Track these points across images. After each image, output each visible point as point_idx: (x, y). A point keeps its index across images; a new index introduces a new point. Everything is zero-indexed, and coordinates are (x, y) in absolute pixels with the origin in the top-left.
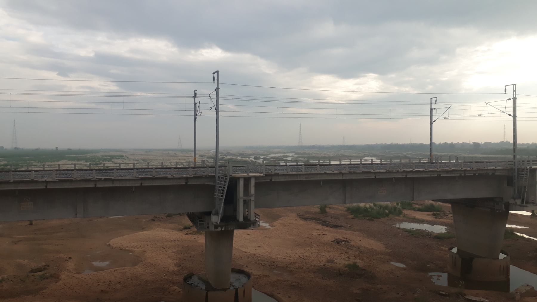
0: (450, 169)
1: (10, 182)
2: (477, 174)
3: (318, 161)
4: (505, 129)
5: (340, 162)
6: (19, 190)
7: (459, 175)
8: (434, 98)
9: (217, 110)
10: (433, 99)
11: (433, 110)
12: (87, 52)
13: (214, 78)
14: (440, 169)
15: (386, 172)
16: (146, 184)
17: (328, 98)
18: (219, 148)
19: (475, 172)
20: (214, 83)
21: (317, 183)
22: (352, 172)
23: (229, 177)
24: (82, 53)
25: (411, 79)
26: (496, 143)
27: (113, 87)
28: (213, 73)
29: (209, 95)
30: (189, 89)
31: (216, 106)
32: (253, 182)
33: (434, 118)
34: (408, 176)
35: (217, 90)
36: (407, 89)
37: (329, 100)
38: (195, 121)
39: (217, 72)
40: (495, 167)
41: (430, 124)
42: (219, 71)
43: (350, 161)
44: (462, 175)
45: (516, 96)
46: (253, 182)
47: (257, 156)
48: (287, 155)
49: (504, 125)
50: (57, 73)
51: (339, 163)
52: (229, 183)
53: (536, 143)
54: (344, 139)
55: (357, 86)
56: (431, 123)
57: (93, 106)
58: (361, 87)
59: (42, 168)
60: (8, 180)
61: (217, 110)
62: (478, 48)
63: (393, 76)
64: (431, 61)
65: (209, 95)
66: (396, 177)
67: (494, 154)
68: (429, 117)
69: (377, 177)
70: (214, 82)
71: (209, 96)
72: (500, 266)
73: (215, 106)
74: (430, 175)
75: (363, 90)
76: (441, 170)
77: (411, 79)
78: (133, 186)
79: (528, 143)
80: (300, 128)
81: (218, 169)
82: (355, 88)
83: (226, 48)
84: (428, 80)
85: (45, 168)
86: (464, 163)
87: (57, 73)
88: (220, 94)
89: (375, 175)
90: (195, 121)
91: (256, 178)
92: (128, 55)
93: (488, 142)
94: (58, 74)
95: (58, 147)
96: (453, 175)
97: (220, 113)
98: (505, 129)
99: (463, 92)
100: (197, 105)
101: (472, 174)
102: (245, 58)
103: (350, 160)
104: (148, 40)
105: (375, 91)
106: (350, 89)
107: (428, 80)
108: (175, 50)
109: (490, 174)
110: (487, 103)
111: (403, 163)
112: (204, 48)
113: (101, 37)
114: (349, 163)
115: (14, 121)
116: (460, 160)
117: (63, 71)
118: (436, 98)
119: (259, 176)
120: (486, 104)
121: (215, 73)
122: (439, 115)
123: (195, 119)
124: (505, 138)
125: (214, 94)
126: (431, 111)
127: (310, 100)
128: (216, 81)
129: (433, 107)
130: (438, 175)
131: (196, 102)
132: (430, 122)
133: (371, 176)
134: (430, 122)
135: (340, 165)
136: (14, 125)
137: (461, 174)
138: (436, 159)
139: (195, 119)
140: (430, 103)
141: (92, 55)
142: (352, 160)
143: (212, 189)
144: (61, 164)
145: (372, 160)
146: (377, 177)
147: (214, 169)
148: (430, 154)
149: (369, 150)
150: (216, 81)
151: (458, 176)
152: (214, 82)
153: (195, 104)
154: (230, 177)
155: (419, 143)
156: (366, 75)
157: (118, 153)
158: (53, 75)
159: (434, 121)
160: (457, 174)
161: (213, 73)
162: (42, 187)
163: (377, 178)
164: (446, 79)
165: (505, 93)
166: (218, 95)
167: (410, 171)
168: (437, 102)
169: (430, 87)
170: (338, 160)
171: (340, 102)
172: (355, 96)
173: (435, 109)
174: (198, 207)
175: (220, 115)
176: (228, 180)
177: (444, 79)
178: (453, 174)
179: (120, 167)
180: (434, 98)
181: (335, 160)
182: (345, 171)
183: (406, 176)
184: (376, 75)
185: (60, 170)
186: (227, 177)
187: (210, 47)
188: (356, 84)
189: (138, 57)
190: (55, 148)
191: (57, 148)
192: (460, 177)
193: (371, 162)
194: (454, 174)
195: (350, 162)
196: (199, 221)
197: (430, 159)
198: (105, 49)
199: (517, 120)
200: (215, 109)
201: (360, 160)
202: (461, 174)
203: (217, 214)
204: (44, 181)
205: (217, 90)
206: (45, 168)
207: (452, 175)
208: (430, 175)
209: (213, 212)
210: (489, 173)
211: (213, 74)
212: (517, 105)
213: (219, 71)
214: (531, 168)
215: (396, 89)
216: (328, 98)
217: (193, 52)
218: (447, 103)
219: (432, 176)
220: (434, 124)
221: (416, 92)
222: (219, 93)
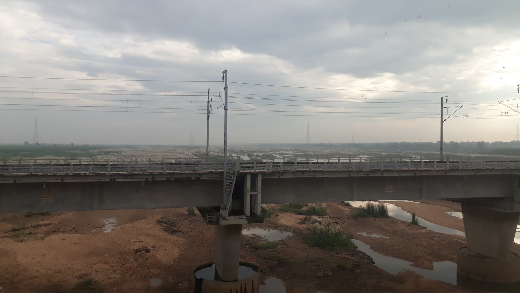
0: (128, 172)
1: (447, 170)
2: (172, 179)
3: (305, 159)
4: (517, 128)
5: (329, 160)
6: (467, 176)
7: (144, 180)
8: (445, 97)
9: (226, 109)
10: (443, 98)
11: (444, 109)
12: (114, 54)
13: (223, 77)
14: (111, 173)
15: (27, 176)
16: (418, 174)
17: (345, 97)
18: (228, 145)
19: (169, 177)
20: (223, 81)
21: (39, 185)
22: (373, 170)
23: (236, 173)
24: (110, 54)
25: (427, 78)
26: (507, 143)
27: (138, 87)
28: (223, 73)
29: (220, 94)
30: (204, 87)
31: (224, 105)
32: (260, 179)
33: (445, 117)
34: (65, 181)
35: (226, 88)
36: (424, 88)
37: (345, 99)
38: (208, 119)
39: (226, 71)
40: (199, 171)
41: (440, 123)
42: (227, 70)
43: (350, 160)
44: (149, 180)
45: (227, 85)
46: (260, 179)
47: (251, 153)
48: (283, 153)
49: (308, 122)
50: (87, 73)
51: (348, 161)
52: (236, 178)
53: (518, 143)
54: (353, 137)
55: (373, 85)
56: (442, 122)
57: (120, 104)
58: (377, 86)
59: (338, 160)
60: (309, 169)
61: (226, 109)
62: (496, 47)
63: (409, 75)
64: (448, 61)
65: (220, 94)
66: (47, 181)
67: (488, 154)
68: (440, 116)
69: (17, 182)
70: (223, 80)
71: (219, 95)
72: (231, 290)
73: (224, 104)
74: (100, 180)
75: (380, 89)
76: (112, 173)
77: (427, 78)
78: (325, 178)
79: (432, 141)
80: (308, 126)
81: (226, 166)
82: (371, 87)
83: (244, 49)
84: (445, 80)
85: (6, 163)
86: (327, 163)
87: (87, 73)
88: (228, 92)
89: (14, 180)
90: (208, 119)
91: (263, 174)
92: (153, 56)
93: (498, 142)
94: (87, 75)
95: (73, 142)
96: (136, 180)
97: (228, 112)
98: (517, 128)
99: (481, 91)
100: (210, 103)
101: (165, 179)
102: (263, 58)
103: (339, 158)
104: (171, 43)
105: (391, 90)
106: (367, 88)
107: (445, 80)
108: (196, 51)
109: (192, 179)
110: (500, 102)
111: (342, 163)
112: (224, 49)
113: (128, 39)
114: (327, 161)
115: (36, 118)
116: (432, 159)
117: (93, 71)
118: (446, 97)
119: (16, 175)
120: (499, 103)
121: (224, 73)
122: (450, 114)
123: (208, 116)
124: (518, 137)
125: (223, 94)
126: (441, 110)
127: (326, 99)
128: (225, 80)
129: (444, 107)
130: (111, 180)
131: (209, 101)
132: (441, 121)
133: (21, 180)
134: (440, 121)
135: (318, 163)
136: (36, 122)
137: (147, 179)
138: (447, 158)
139: (208, 116)
140: (441, 102)
141: (119, 56)
142: (340, 159)
143: (221, 183)
144: (362, 157)
145: (361, 158)
146: (17, 182)
147: (223, 165)
148: (441, 153)
149: (362, 148)
150: (225, 80)
151: (144, 181)
152: (223, 80)
153: (208, 102)
154: (237, 173)
155: (429, 142)
156: (383, 74)
157: (113, 150)
158: (83, 75)
159: (445, 120)
160: (142, 178)
161: (223, 73)
162: (12, 181)
163: (17, 183)
164: (463, 78)
165: (519, 93)
166: (226, 93)
167: (194, 172)
168: (448, 100)
169: (447, 86)
170: (326, 158)
171: (356, 101)
172: (371, 95)
173: (445, 108)
174: (207, 203)
175: (228, 113)
176: (236, 175)
177: (461, 78)
178: (135, 179)
179: (412, 160)
180: (445, 97)
181: (322, 158)
182: (421, 168)
183: (62, 181)
184: (392, 75)
185: (80, 165)
186: (234, 172)
187: (229, 48)
188: (373, 83)
189: (163, 58)
190: (71, 144)
191: (72, 143)
192: (147, 182)
193: (317, 161)
194: (137, 178)
195: (338, 160)
196: (208, 215)
197: (441, 158)
198: (131, 51)
199: (444, 117)
200: (224, 107)
201: (349, 159)
202: (147, 179)
203: (225, 208)
204: (179, 173)
205: (226, 88)
206: (6, 163)
207: (133, 180)
208: (100, 180)
209: (222, 206)
210: (191, 178)
211: (223, 74)
212: (228, 95)
213: (227, 70)
214: (239, 173)
215: (412, 88)
216: (345, 97)
217: (213, 53)
218: (460, 103)
219: (103, 180)
220: (444, 123)
221: (433, 91)
222: (227, 91)
